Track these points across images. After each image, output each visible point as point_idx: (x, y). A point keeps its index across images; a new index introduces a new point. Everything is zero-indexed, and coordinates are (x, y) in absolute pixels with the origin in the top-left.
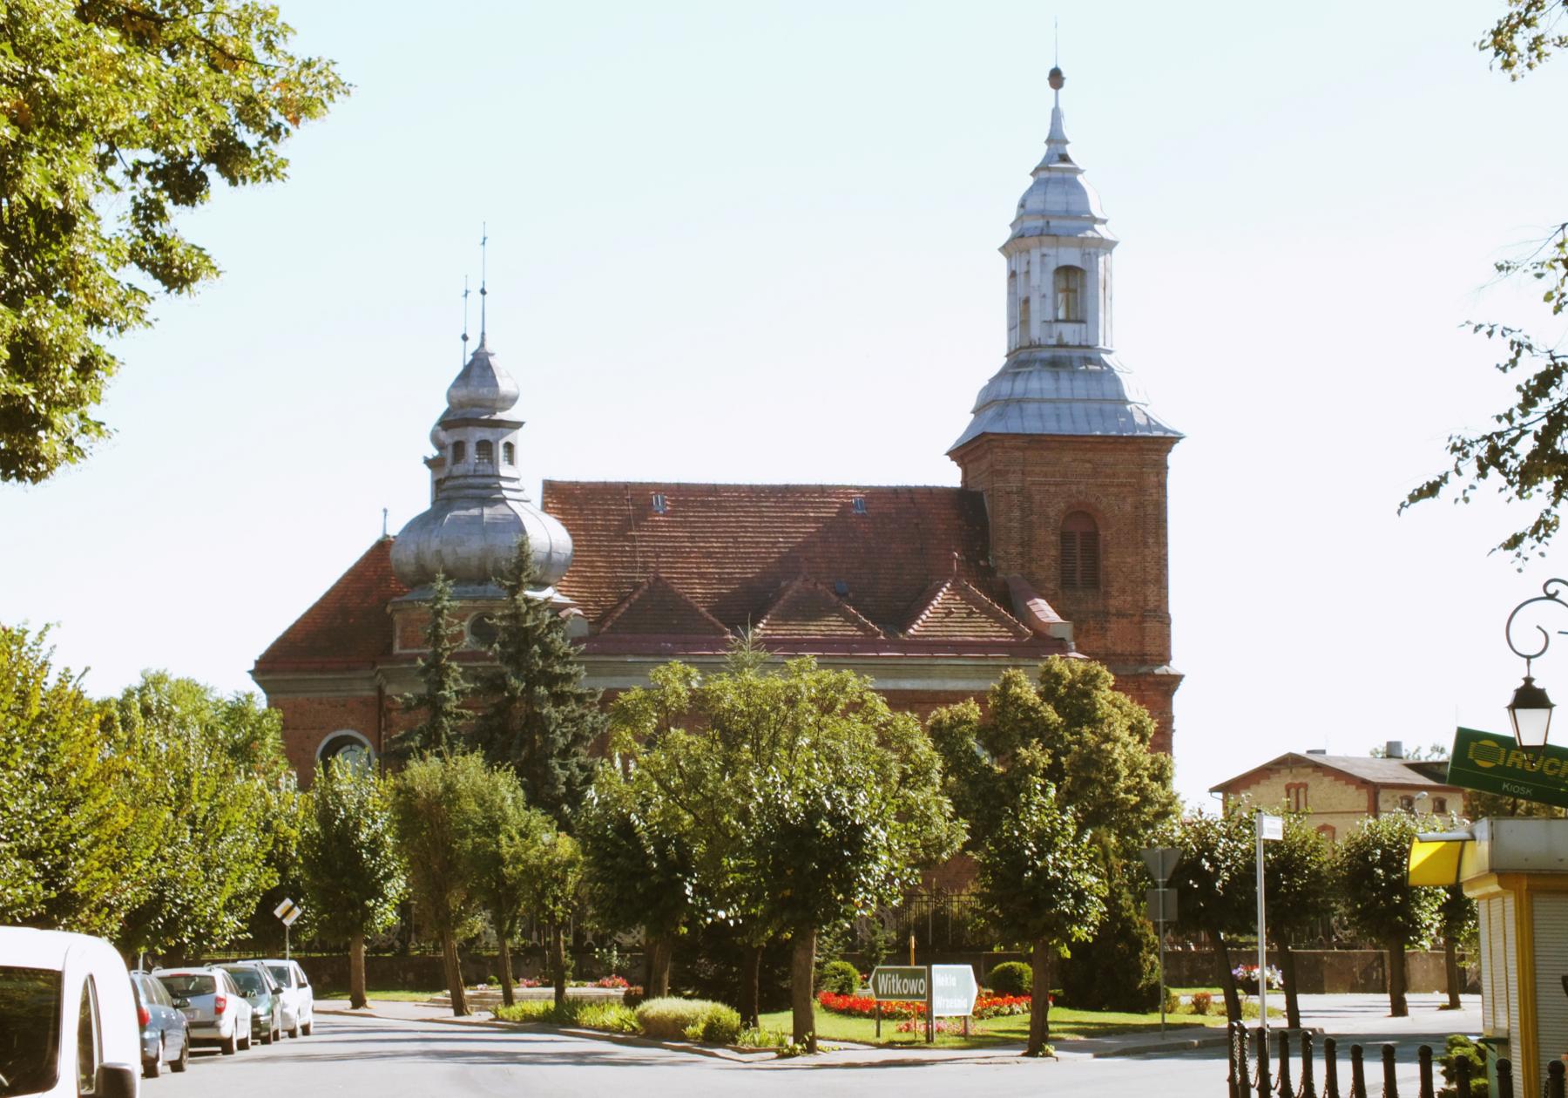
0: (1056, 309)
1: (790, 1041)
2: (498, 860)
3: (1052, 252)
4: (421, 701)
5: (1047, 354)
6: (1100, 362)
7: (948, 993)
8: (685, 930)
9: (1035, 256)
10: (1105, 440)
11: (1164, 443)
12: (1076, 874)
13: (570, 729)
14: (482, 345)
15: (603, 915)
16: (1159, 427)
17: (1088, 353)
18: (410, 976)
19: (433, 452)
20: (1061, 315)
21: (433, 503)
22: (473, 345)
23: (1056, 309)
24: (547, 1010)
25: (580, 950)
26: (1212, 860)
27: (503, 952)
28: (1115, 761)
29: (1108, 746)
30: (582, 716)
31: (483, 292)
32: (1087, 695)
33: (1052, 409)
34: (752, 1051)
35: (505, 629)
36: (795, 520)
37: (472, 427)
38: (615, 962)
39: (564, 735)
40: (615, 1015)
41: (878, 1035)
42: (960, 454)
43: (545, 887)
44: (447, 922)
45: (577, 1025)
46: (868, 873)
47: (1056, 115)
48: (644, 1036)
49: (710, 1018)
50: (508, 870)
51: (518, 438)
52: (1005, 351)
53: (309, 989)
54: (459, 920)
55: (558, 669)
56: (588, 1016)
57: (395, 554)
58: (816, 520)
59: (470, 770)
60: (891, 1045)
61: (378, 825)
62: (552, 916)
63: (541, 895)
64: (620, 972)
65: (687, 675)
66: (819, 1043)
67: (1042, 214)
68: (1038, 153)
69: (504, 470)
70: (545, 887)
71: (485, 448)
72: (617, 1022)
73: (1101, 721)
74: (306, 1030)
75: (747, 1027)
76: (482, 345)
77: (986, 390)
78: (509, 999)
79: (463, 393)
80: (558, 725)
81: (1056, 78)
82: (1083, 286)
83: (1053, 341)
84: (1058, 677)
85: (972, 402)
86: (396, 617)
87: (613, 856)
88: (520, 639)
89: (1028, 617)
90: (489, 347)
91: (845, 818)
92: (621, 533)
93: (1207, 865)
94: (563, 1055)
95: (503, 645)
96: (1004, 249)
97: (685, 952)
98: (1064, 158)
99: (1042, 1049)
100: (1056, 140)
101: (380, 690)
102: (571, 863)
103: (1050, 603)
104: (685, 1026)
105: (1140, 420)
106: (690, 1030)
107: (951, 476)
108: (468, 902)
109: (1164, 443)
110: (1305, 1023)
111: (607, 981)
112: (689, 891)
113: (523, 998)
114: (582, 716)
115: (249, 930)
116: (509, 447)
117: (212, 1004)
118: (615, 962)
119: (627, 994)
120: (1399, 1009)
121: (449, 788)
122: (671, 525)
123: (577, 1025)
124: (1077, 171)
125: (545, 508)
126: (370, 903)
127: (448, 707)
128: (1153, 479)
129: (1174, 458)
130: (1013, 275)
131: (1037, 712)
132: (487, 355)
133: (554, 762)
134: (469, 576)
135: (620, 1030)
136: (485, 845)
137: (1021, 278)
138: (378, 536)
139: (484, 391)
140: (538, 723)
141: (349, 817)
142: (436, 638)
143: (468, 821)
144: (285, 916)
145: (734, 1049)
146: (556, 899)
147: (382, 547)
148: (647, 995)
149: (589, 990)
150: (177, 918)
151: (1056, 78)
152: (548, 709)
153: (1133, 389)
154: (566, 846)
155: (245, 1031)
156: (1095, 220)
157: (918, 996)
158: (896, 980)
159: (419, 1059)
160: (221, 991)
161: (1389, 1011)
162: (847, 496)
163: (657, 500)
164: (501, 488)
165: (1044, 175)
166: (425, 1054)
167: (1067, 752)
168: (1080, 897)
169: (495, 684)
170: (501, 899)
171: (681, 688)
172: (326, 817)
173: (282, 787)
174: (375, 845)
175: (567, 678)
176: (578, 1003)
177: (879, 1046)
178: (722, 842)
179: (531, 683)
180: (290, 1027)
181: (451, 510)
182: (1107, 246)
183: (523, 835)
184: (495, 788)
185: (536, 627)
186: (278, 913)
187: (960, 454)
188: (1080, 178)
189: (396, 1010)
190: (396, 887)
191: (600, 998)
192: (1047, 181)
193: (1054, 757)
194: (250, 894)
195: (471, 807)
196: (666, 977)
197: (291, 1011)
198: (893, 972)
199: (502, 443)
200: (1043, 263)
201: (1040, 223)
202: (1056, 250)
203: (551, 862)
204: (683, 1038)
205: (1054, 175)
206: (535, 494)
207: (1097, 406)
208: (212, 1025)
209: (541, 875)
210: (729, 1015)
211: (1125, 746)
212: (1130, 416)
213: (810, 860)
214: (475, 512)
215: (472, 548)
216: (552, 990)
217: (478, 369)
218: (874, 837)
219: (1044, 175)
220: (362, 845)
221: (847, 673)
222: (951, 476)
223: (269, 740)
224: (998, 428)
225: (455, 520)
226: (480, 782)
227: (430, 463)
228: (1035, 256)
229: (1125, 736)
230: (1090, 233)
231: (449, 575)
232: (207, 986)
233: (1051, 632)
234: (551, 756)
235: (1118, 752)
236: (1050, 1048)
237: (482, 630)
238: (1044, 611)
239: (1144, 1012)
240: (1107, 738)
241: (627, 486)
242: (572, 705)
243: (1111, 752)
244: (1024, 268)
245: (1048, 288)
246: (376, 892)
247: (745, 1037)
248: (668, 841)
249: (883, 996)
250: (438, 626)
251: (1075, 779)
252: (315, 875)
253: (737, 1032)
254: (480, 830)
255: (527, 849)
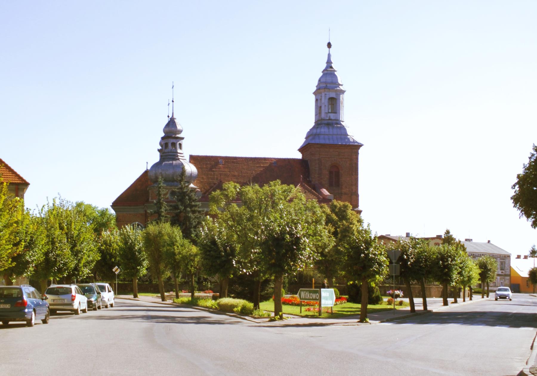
0: (329, 109)
1: (273, 315)
2: (174, 254)
3: (328, 93)
4: (155, 212)
5: (326, 122)
6: (341, 124)
7: (326, 299)
8: (232, 276)
9: (323, 94)
10: (342, 145)
11: (359, 146)
12: (379, 256)
13: (197, 220)
14: (173, 116)
15: (206, 270)
16: (357, 142)
17: (337, 122)
18: (152, 289)
19: (160, 148)
20: (330, 111)
21: (160, 159)
22: (171, 116)
23: (329, 109)
24: (189, 300)
25: (199, 282)
26: (407, 255)
27: (176, 282)
28: (353, 230)
29: (352, 226)
30: (200, 217)
31: (173, 101)
32: (345, 211)
33: (327, 136)
34: (258, 318)
35: (178, 192)
36: (257, 167)
37: (171, 137)
38: (209, 286)
39: (195, 222)
40: (210, 303)
41: (301, 312)
42: (301, 150)
43: (188, 262)
44: (159, 273)
45: (198, 305)
46: (302, 255)
47: (329, 55)
48: (219, 310)
49: (243, 305)
50: (177, 257)
51: (183, 142)
52: (314, 121)
53: (112, 292)
54: (163, 273)
55: (193, 203)
56: (202, 303)
57: (149, 174)
58: (263, 167)
59: (166, 228)
60: (306, 316)
61: (139, 245)
62: (190, 271)
63: (187, 265)
64: (211, 289)
65: (235, 186)
66: (284, 316)
67: (325, 83)
68: (324, 66)
69: (179, 151)
70: (188, 262)
71: (174, 145)
72: (210, 305)
73: (349, 219)
74: (112, 305)
75: (256, 309)
76: (173, 116)
77: (309, 133)
78: (177, 297)
79: (167, 129)
80: (193, 219)
81: (329, 45)
82: (336, 103)
83: (328, 118)
84: (336, 206)
85: (305, 136)
86: (150, 191)
87: (210, 251)
88: (183, 196)
89: (321, 194)
90: (175, 117)
91: (294, 234)
92: (211, 169)
93: (405, 257)
94: (192, 318)
95: (178, 196)
96: (314, 93)
97: (231, 283)
98: (331, 67)
99: (365, 320)
100: (329, 62)
101: (146, 211)
102: (196, 255)
103: (327, 190)
104: (234, 308)
105: (351, 140)
106: (235, 309)
107: (299, 156)
108: (166, 267)
109: (359, 146)
110: (429, 308)
111: (207, 291)
112: (234, 262)
113: (182, 296)
114: (200, 217)
115: (92, 273)
116: (180, 145)
117: (70, 298)
118: (209, 286)
119: (213, 296)
120: (446, 303)
121: (160, 233)
122: (224, 167)
123: (198, 305)
124: (335, 71)
125: (190, 162)
126: (139, 268)
127: (163, 214)
128: (355, 157)
129: (361, 151)
130: (317, 100)
131: (330, 216)
132: (174, 119)
133: (192, 230)
134: (169, 180)
135: (211, 308)
136: (170, 249)
137: (319, 101)
138: (145, 169)
139: (173, 129)
140: (188, 218)
141: (132, 242)
142: (159, 195)
143: (165, 242)
144: (116, 271)
145: (252, 317)
146: (192, 266)
147: (146, 172)
148: (220, 297)
149: (202, 294)
150: (62, 268)
151: (329, 45)
152: (190, 215)
153: (350, 132)
154: (194, 249)
155: (84, 306)
156: (340, 85)
157: (316, 299)
158: (308, 294)
159: (139, 320)
160: (73, 293)
161: (442, 304)
162: (271, 160)
163: (220, 161)
164: (178, 156)
165: (326, 72)
166: (143, 317)
167: (339, 227)
168: (380, 265)
169: (176, 208)
170: (175, 266)
171: (234, 190)
172: (126, 243)
173: (115, 234)
174: (140, 251)
175: (196, 206)
176: (199, 298)
177: (302, 317)
178: (247, 245)
179: (186, 207)
180: (106, 305)
181: (164, 161)
182: (343, 92)
183: (182, 246)
184: (173, 232)
185: (187, 191)
186: (114, 270)
187: (301, 150)
188: (335, 73)
189: (147, 299)
190: (146, 263)
191: (205, 296)
192: (327, 74)
193: (336, 229)
194: (92, 261)
195: (166, 238)
196: (226, 291)
197: (106, 299)
198: (307, 291)
199: (178, 143)
200: (325, 97)
201: (324, 85)
202: (329, 92)
203: (190, 254)
204: (233, 312)
205: (329, 72)
206: (188, 158)
207: (339, 136)
208: (71, 305)
209: (187, 258)
210: (251, 305)
211: (356, 226)
212: (349, 139)
213: (281, 249)
214: (171, 162)
215: (170, 172)
216: (190, 294)
217: (172, 123)
218: (304, 241)
219: (326, 72)
220: (136, 251)
221: (292, 186)
222: (299, 156)
223: (112, 222)
224: (313, 142)
225: (165, 164)
226: (168, 229)
227: (159, 150)
228: (323, 94)
229: (356, 223)
230: (338, 88)
231: (166, 180)
232: (69, 291)
233: (328, 197)
234: (191, 228)
235: (354, 228)
236: (368, 320)
237: (173, 193)
238: (325, 192)
239: (374, 304)
240: (351, 223)
241: (212, 157)
242: (197, 214)
243: (352, 228)
244: (320, 98)
245: (327, 104)
246: (140, 264)
247: (256, 313)
248: (227, 246)
249: (303, 299)
250: (160, 191)
251: (341, 235)
252: (123, 259)
253: (252, 311)
254: (168, 245)
255: (183, 250)
